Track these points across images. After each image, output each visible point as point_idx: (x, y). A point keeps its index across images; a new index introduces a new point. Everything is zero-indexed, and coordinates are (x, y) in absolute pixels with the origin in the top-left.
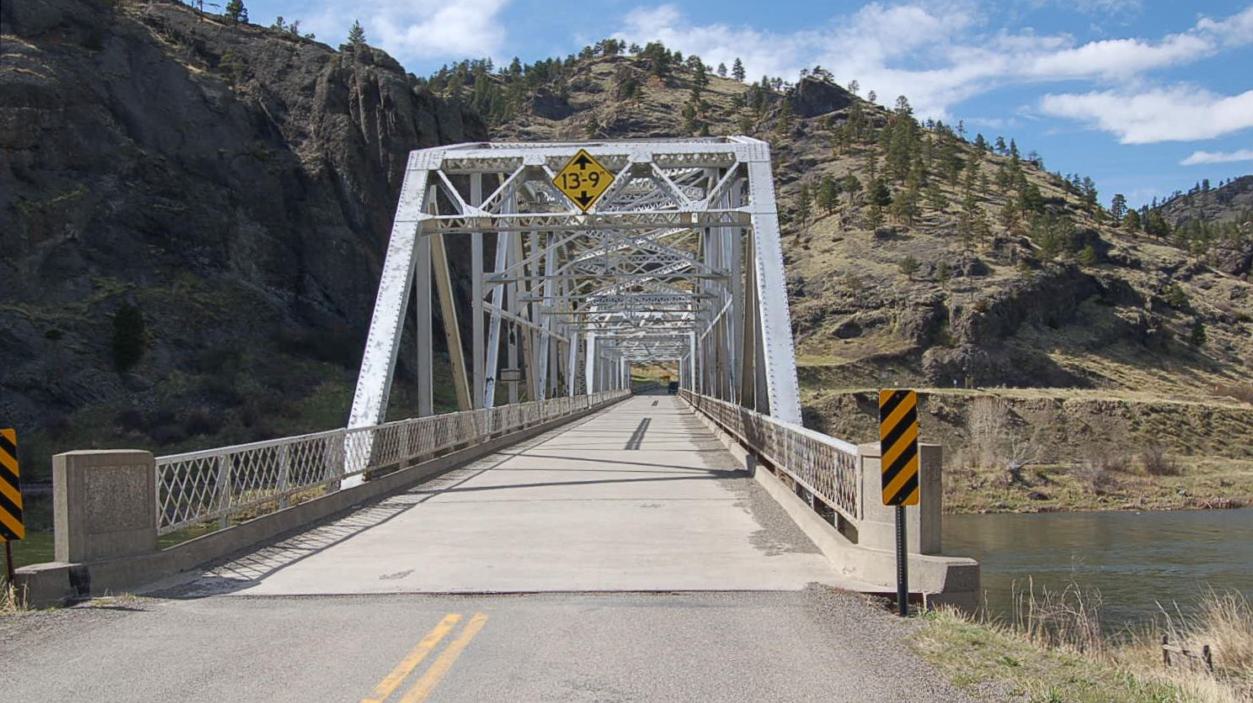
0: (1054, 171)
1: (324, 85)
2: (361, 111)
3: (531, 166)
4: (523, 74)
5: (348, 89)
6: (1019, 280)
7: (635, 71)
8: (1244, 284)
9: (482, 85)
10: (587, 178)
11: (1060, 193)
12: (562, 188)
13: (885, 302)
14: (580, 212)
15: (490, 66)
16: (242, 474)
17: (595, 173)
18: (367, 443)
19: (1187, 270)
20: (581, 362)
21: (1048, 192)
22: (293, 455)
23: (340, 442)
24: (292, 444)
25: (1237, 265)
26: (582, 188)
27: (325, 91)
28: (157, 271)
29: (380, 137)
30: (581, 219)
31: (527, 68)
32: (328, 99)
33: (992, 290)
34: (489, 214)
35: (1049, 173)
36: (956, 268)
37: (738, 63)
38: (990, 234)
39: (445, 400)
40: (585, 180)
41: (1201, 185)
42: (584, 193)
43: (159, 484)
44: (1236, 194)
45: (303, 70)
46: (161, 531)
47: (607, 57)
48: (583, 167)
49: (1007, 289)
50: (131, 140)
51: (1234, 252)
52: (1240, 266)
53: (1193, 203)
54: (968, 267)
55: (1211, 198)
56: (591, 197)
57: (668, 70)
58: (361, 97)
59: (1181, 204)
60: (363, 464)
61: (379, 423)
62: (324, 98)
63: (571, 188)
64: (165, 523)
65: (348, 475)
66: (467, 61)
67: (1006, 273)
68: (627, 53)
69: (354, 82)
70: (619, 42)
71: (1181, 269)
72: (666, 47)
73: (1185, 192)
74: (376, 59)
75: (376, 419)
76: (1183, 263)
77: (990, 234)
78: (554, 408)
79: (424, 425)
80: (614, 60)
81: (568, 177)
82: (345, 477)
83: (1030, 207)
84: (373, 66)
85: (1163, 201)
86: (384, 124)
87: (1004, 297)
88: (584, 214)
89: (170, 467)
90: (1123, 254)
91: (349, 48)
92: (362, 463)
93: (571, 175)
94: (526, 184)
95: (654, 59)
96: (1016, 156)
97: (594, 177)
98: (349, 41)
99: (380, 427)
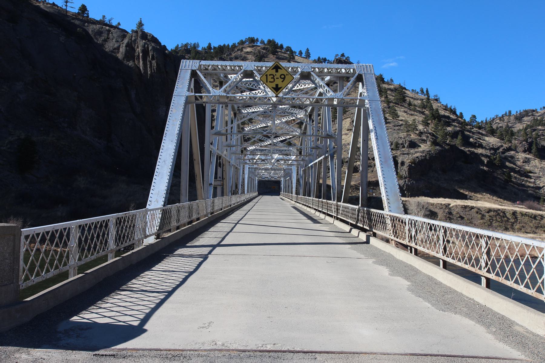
0: (445, 104)
1: (124, 48)
2: (141, 60)
3: (247, 71)
4: (212, 51)
5: (135, 51)
6: (430, 151)
7: (262, 52)
8: (528, 156)
9: (194, 54)
10: (279, 77)
11: (447, 114)
12: (265, 82)
13: (370, 158)
14: (275, 95)
15: (198, 46)
16: (86, 239)
17: (284, 75)
18: (158, 217)
19: (503, 150)
20: (243, 178)
21: (442, 112)
22: (118, 225)
23: (145, 216)
24: (118, 218)
25: (525, 148)
26: (276, 82)
27: (124, 51)
28: (42, 129)
29: (149, 73)
30: (274, 99)
31: (215, 48)
32: (125, 54)
33: (418, 155)
34: (225, 94)
35: (443, 105)
36: (402, 144)
37: (308, 50)
38: (417, 130)
39: (193, 197)
40: (277, 78)
41: (508, 113)
42: (277, 85)
43: (23, 250)
44: (523, 117)
45: (114, 40)
46: (23, 285)
47: (249, 45)
48: (277, 71)
49: (424, 155)
50: (31, 67)
51: (523, 143)
52: (526, 149)
53: (503, 120)
54: (407, 144)
55: (512, 118)
56: (281, 87)
57: (277, 52)
58: (141, 54)
59: (498, 121)
60: (155, 229)
61: (164, 206)
62: (124, 54)
63: (270, 82)
64: (27, 279)
65: (148, 236)
66: (188, 43)
67: (424, 147)
68: (259, 44)
69: (138, 47)
70: (256, 38)
71: (501, 149)
72: (277, 41)
73: (500, 115)
74: (148, 37)
75: (163, 203)
76: (502, 146)
77: (417, 130)
78: (235, 200)
79: (183, 207)
80: (253, 46)
81: (268, 76)
82: (146, 237)
83: (434, 119)
84: (147, 41)
85: (490, 119)
86: (151, 67)
87: (423, 158)
88: (276, 96)
89: (33, 235)
90: (475, 141)
91: (136, 32)
92: (155, 229)
93: (270, 75)
94: (264, 67)
95: (271, 46)
96: (429, 97)
97: (283, 77)
98: (136, 29)
99: (165, 208)
